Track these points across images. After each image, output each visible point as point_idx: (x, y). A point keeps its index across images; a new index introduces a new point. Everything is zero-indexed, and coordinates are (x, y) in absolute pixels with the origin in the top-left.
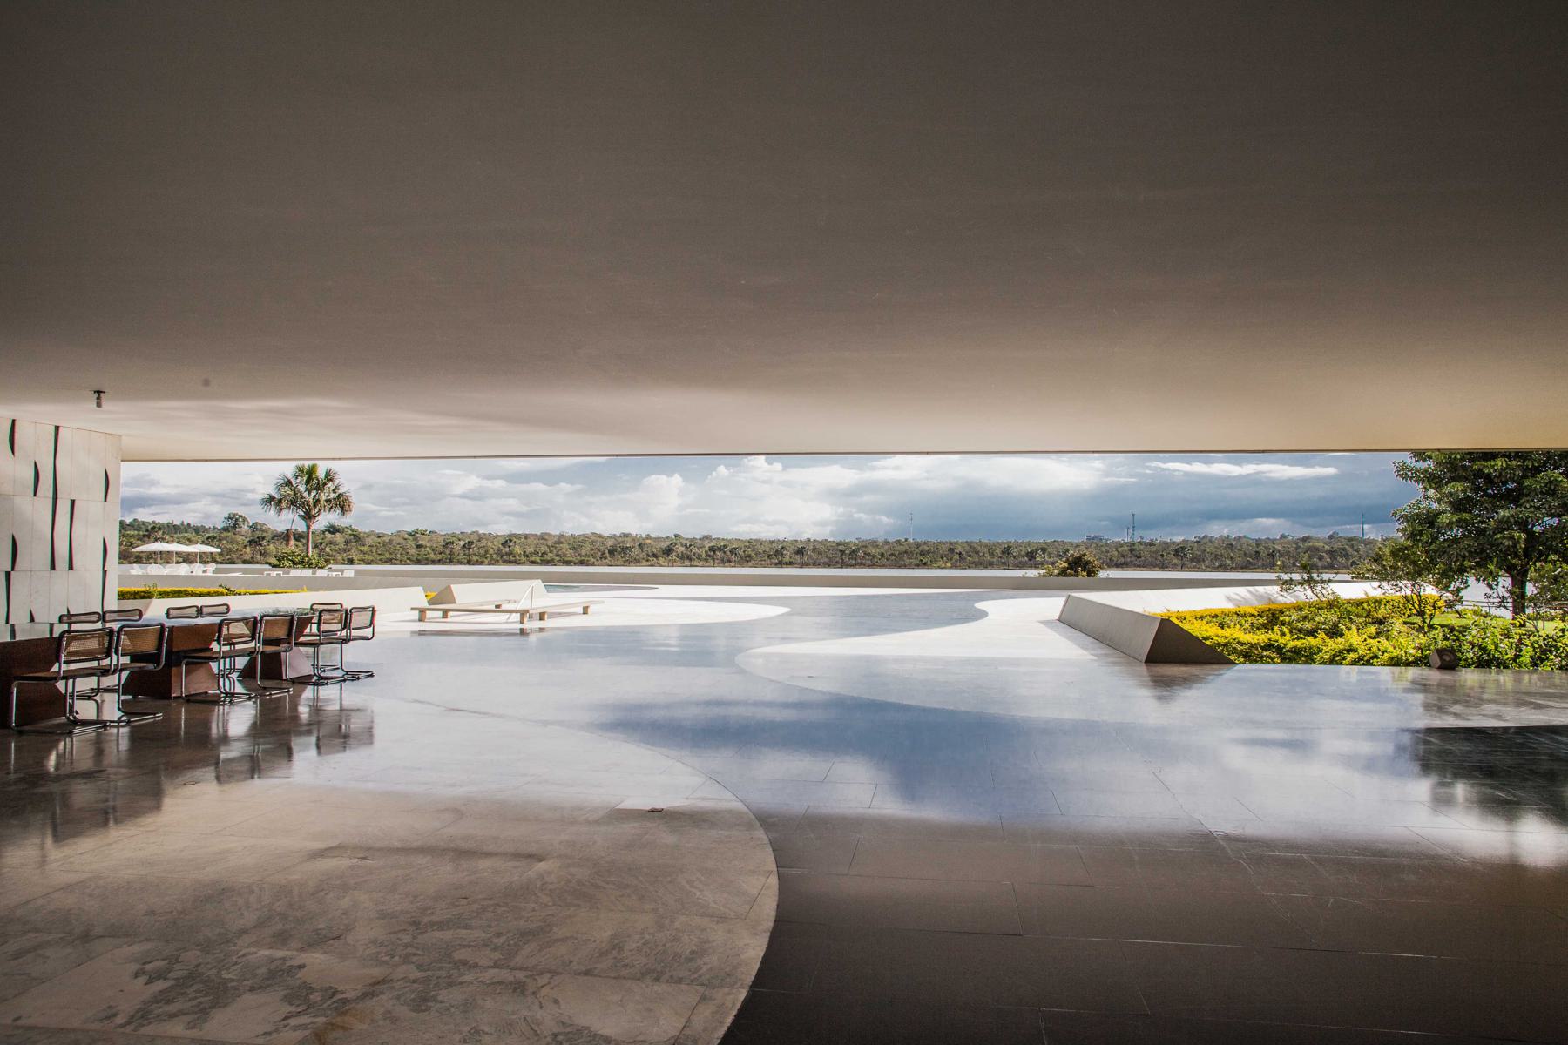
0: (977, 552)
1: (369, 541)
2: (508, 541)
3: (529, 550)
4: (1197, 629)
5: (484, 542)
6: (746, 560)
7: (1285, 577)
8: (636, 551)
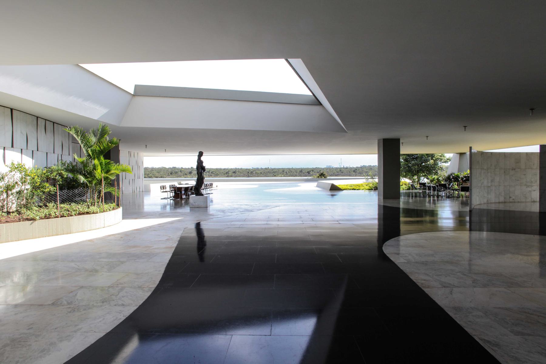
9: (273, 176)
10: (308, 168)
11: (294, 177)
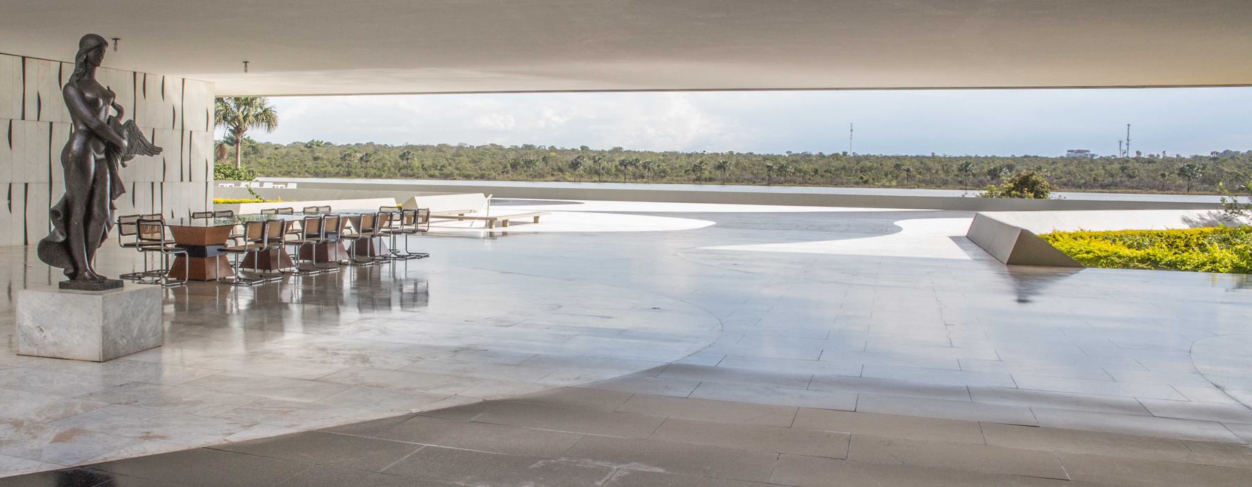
0: (929, 169)
1: (268, 152)
2: (406, 153)
3: (428, 163)
4: (1061, 246)
5: (381, 154)
6: (661, 176)
7: (1229, 200)
8: (540, 164)
9: (857, 184)
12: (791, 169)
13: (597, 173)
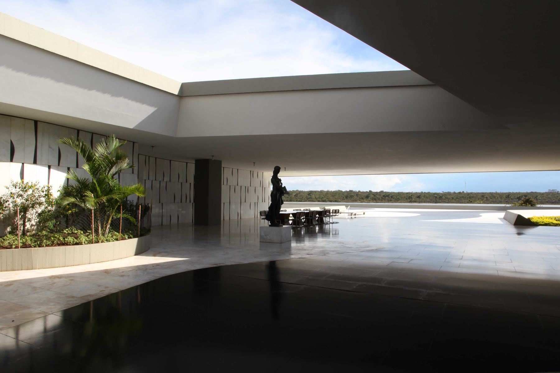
0: (495, 197)
2: (310, 193)
3: (317, 197)
4: (534, 220)
8: (355, 197)
9: (468, 203)
10: (519, 193)
11: (498, 203)
12: (444, 197)
13: (375, 199)
